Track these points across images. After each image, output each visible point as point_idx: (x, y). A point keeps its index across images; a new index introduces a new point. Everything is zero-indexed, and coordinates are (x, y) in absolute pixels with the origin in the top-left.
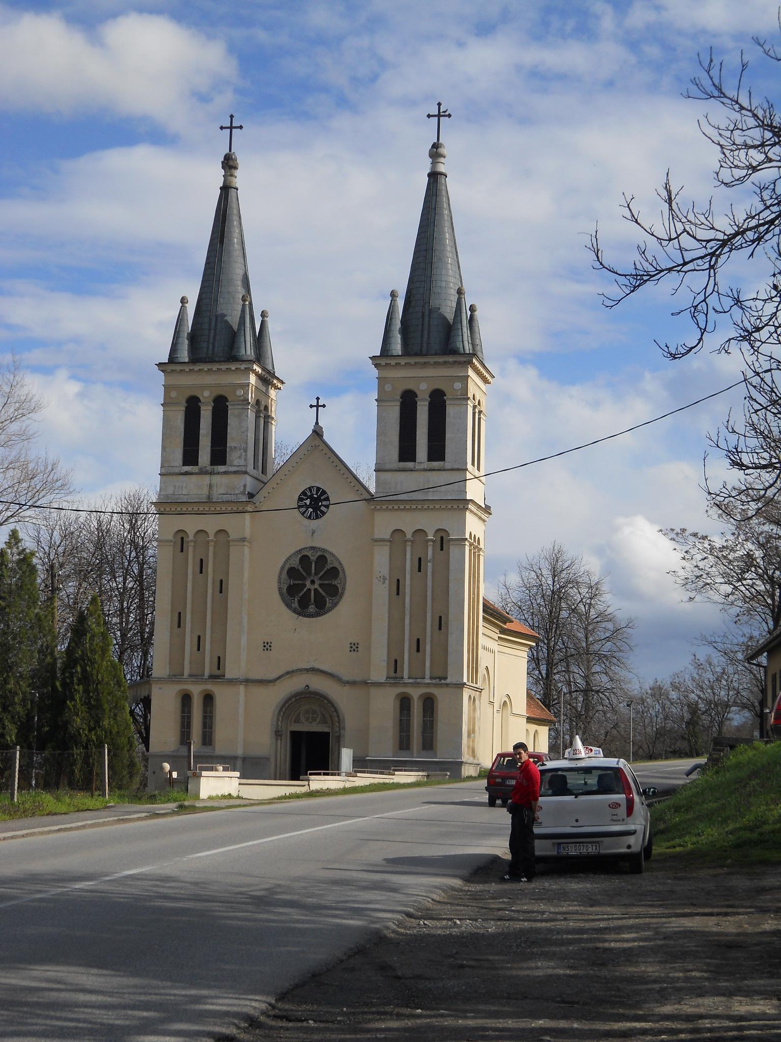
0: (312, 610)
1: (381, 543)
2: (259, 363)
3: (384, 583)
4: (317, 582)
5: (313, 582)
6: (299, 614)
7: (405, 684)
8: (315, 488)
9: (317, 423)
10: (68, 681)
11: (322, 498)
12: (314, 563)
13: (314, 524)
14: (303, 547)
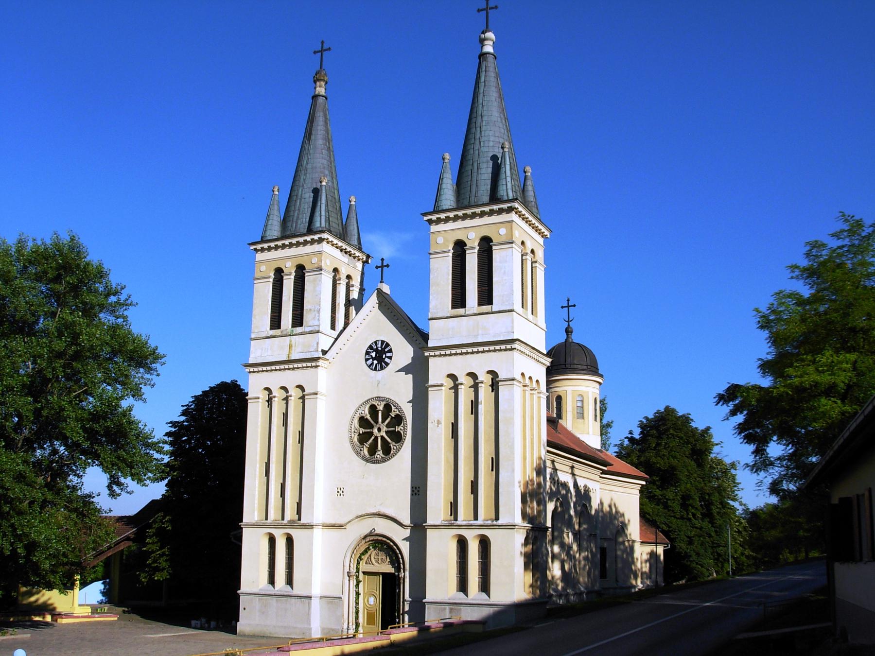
2: (343, 235)
5: (379, 430)
6: (367, 461)
8: (380, 342)
10: (656, 497)
11: (386, 350)
14: (370, 397)
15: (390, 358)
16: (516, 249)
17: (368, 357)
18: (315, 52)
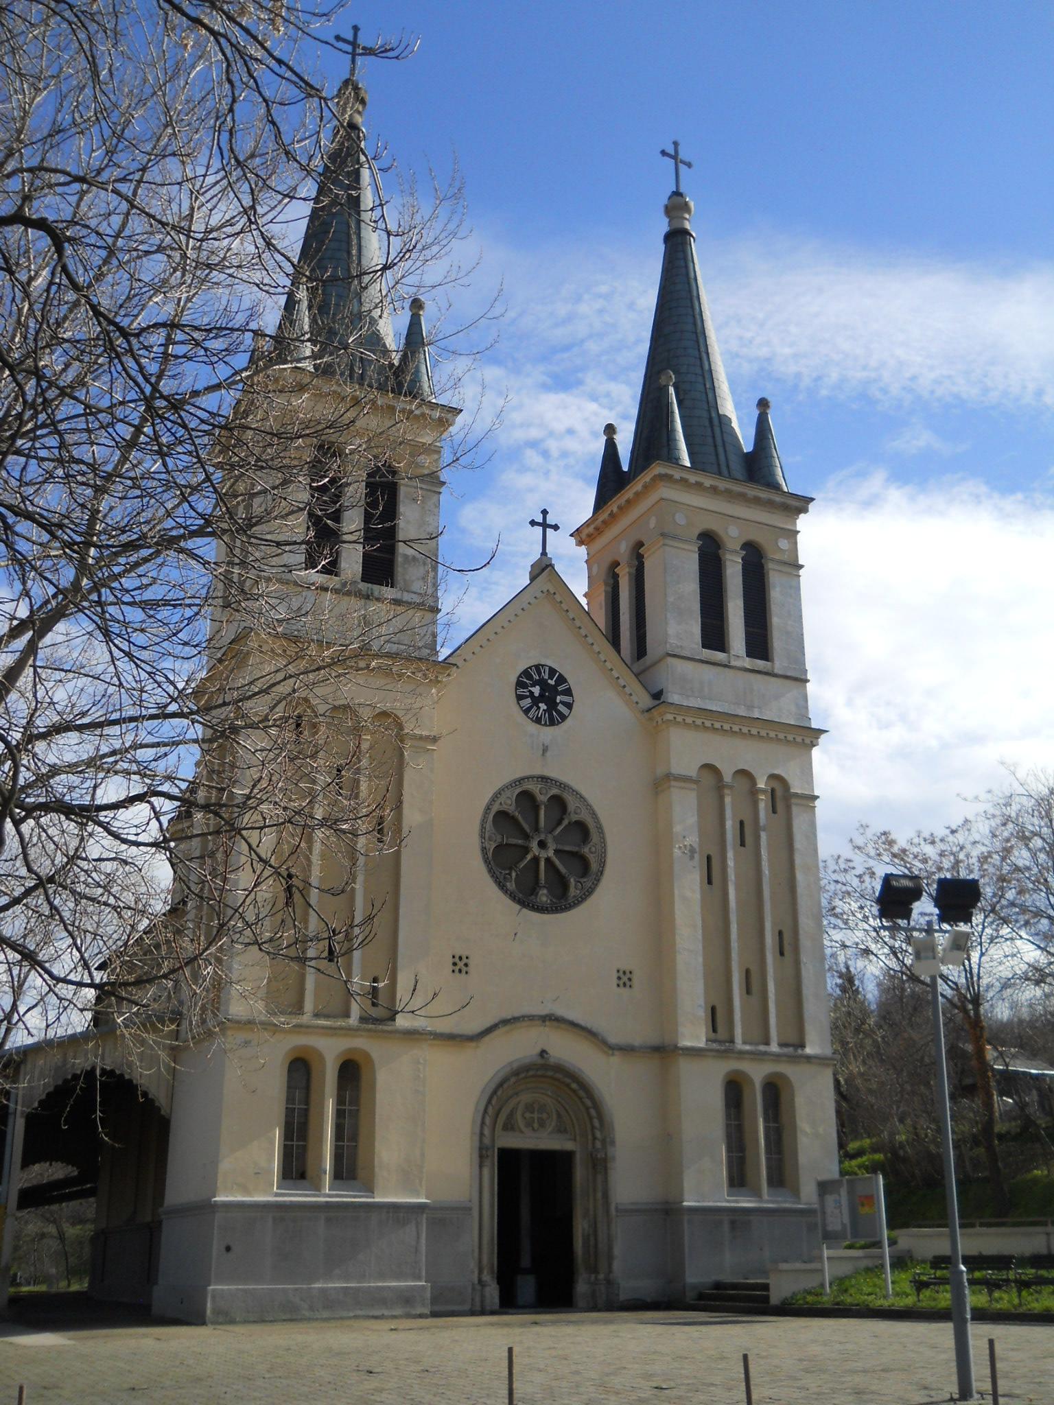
0: (544, 899)
1: (683, 784)
3: (692, 858)
4: (552, 847)
5: (542, 845)
7: (741, 1054)
9: (544, 553)
12: (543, 807)
13: (548, 734)
15: (569, 706)
16: (288, 259)
17: (527, 702)
18: (356, 29)
